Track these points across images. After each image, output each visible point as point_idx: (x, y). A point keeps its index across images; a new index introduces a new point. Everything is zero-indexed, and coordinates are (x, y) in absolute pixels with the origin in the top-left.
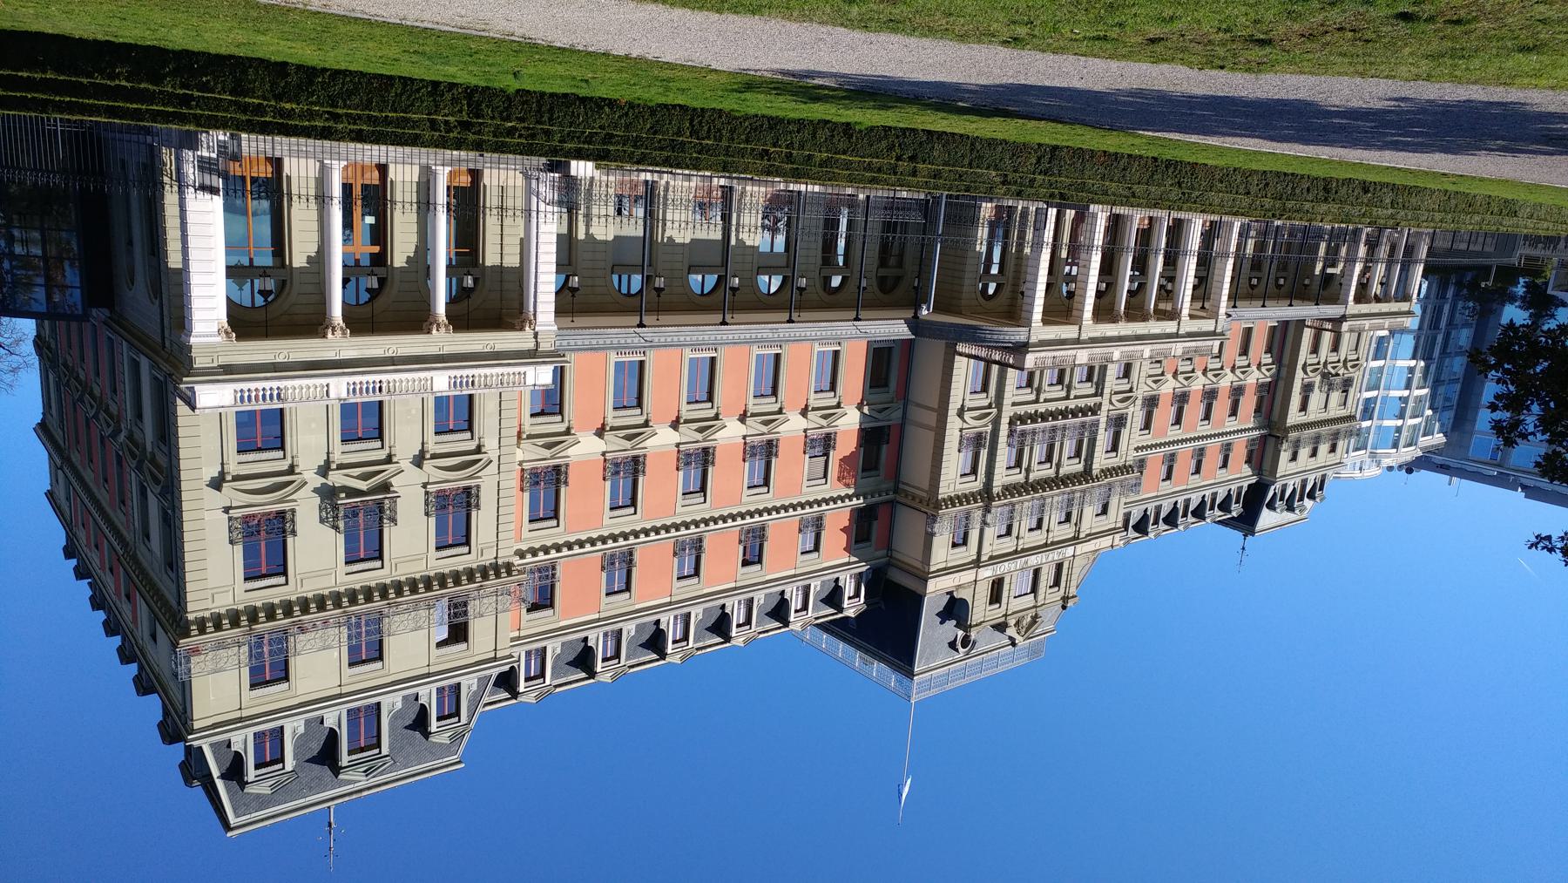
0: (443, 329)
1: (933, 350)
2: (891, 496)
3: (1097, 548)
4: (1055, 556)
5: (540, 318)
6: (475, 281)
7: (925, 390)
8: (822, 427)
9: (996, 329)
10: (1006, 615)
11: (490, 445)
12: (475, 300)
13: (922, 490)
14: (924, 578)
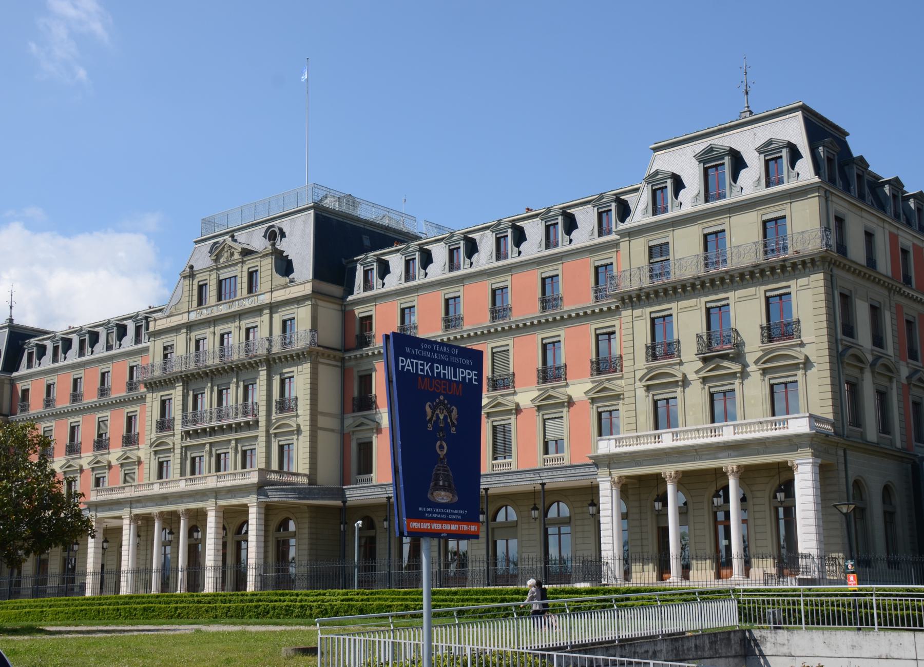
0: (668, 474)
1: (328, 476)
2: (347, 355)
3: (169, 319)
4: (205, 313)
5: (608, 485)
6: (775, 497)
7: (329, 444)
8: (608, 380)
9: (283, 499)
10: (243, 262)
11: (641, 392)
12: (775, 483)
13: (323, 363)
14: (316, 293)
